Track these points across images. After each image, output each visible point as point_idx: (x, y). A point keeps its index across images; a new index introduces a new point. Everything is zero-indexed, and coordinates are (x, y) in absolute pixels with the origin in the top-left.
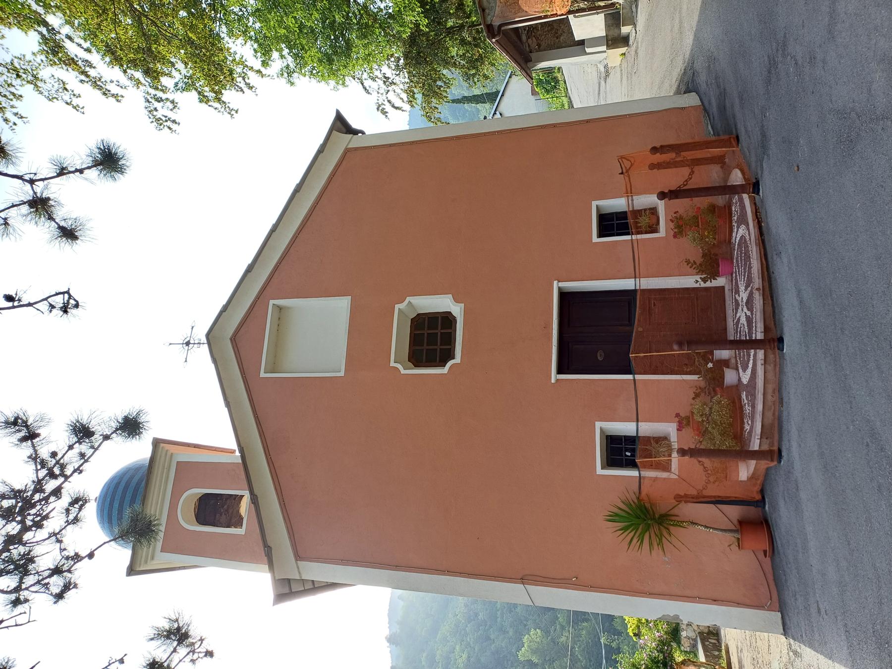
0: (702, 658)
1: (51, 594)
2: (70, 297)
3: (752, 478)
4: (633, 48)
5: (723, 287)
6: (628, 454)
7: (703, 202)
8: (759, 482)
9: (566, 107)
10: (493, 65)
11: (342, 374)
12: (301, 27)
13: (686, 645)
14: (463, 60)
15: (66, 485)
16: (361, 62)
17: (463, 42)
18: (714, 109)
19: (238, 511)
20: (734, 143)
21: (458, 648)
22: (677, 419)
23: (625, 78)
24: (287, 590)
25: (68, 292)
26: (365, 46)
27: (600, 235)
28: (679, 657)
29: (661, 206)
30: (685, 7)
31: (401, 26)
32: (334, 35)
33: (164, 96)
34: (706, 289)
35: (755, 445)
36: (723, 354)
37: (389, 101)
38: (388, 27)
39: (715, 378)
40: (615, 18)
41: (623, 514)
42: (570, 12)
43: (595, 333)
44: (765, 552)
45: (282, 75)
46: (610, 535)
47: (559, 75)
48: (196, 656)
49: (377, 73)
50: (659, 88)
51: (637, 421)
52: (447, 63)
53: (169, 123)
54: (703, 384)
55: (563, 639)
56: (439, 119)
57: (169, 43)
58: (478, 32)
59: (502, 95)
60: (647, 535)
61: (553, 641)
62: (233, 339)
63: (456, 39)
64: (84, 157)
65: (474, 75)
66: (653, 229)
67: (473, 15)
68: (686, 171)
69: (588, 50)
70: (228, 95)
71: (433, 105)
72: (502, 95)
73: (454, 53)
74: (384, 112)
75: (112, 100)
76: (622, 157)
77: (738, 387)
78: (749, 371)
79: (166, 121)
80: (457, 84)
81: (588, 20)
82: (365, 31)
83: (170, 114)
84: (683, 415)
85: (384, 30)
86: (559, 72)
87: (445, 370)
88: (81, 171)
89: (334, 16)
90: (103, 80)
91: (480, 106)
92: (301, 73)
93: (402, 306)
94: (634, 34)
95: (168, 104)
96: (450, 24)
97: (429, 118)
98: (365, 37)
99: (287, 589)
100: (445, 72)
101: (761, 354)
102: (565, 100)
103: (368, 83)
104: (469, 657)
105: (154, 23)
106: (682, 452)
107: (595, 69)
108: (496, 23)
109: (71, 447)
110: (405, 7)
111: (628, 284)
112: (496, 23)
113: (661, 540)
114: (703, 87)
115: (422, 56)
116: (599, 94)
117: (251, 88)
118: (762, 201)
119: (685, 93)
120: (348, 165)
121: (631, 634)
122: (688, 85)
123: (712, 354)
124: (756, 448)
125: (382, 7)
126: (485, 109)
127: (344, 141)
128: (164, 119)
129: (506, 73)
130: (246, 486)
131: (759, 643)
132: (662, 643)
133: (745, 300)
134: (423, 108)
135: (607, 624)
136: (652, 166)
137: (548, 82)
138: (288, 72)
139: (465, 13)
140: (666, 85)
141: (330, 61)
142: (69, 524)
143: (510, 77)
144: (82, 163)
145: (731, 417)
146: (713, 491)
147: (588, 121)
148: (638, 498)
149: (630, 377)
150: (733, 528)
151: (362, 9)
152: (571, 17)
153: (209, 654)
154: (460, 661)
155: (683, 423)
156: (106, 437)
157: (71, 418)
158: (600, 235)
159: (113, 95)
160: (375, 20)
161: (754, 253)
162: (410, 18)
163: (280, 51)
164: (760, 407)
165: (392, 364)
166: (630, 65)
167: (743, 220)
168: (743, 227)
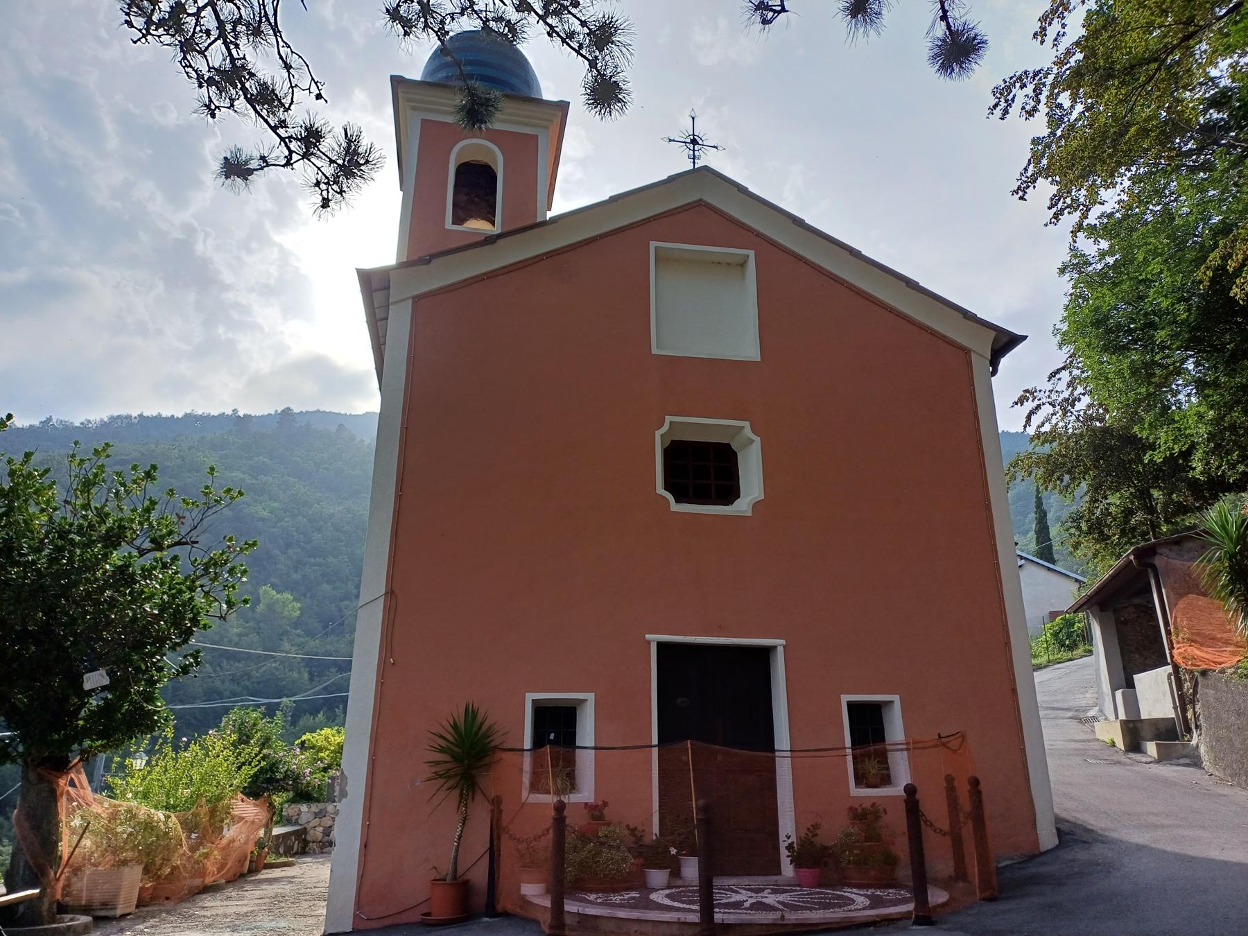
0: (277, 831)
1: (398, 5)
2: (779, 12)
3: (525, 902)
4: (1123, 759)
5: (780, 873)
6: (552, 736)
7: (902, 848)
8: (518, 910)
9: (1034, 661)
10: (1095, 556)
11: (655, 351)
12: (1148, 282)
13: (290, 810)
14: (1102, 514)
15: (533, 18)
16: (1096, 367)
17: (1128, 513)
18: (1033, 869)
19: (471, 217)
20: (987, 894)
21: (276, 505)
22: (600, 803)
23: (1073, 745)
24: (374, 286)
25: (784, 10)
26: (1120, 373)
27: (851, 705)
28: (277, 799)
29: (896, 790)
30: (1186, 832)
31: (1150, 424)
32: (1135, 330)
33: (1043, 98)
34: (777, 848)
35: (571, 907)
36: (691, 869)
37: (1038, 407)
38: (1148, 405)
39: (654, 856)
40: (1169, 734)
41: (475, 729)
42: (1176, 668)
43: (714, 697)
44: (429, 914)
45: (1076, 257)
46: (450, 709)
47: (1080, 651)
48: (323, 186)
49: (1080, 390)
50: (1064, 794)
51: (595, 748)
52: (1096, 489)
53: (1003, 104)
54: (646, 840)
55: (287, 646)
56: (1013, 478)
57: (1121, 101)
58: (1144, 534)
59: (1049, 569)
60: (446, 757)
61: (285, 633)
62: (700, 204)
63: (1133, 503)
64: (963, 20)
65: (1079, 528)
66: (861, 780)
67: (1170, 526)
68: (946, 826)
69: (1119, 693)
70: (1045, 189)
71: (1035, 470)
72: (1049, 569)
73: (1111, 499)
74: (1021, 401)
75: (1036, 27)
76: (964, 737)
77: (645, 888)
78: (668, 902)
79: (1006, 101)
80: (1066, 504)
81: (1164, 695)
82: (1144, 372)
83: (1015, 109)
84: (606, 811)
85: (1145, 399)
86: (1085, 651)
87: (660, 490)
88: (944, 17)
89: (1163, 328)
90: (1066, 14)
91: (1032, 535)
92: (1078, 282)
93: (748, 431)
94: (1144, 760)
95: (1033, 104)
96: (1156, 493)
97: (1015, 465)
98: (1133, 374)
99: (374, 285)
100: (1084, 485)
101: (694, 918)
102: (1043, 660)
103: (1065, 376)
104: (264, 520)
105: (1150, 79)
106: (560, 807)
107: (1091, 702)
108: (1159, 561)
109: (584, 24)
110: (1180, 430)
111: (782, 739)
112: (1159, 561)
113: (441, 776)
114: (1067, 855)
115: (1107, 455)
116: (1054, 709)
117: (1056, 216)
118: (905, 929)
119: (1058, 830)
120: (951, 351)
121: (304, 738)
122: (1069, 834)
123: (692, 854)
124: (567, 908)
125: (1180, 397)
126: (1028, 543)
127: (982, 348)
128: (1010, 97)
129: (1083, 574)
130: (507, 229)
131: (305, 904)
132: (297, 778)
133: (764, 900)
134: (1029, 456)
135: (305, 706)
136: (950, 780)
137: (1069, 636)
138: (1077, 264)
139: (1174, 515)
140: (1069, 804)
141: (1097, 324)
142: (484, 23)
143: (1077, 580)
144: (955, 19)
145: (605, 875)
146: (507, 848)
147: (1014, 691)
148: (496, 747)
149: (655, 741)
150: (459, 874)
151: (1176, 368)
152: (1169, 669)
153: (325, 203)
154: (259, 508)
155: (595, 811)
156: (593, 64)
157: (619, 17)
158: (851, 705)
159: (1044, 29)
160: (1160, 386)
161: (828, 916)
162: (1163, 436)
163: (1111, 252)
164: (622, 914)
165: (668, 419)
166: (1097, 753)
167: (876, 902)
168: (867, 902)
